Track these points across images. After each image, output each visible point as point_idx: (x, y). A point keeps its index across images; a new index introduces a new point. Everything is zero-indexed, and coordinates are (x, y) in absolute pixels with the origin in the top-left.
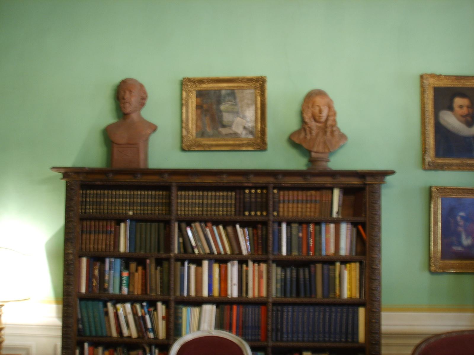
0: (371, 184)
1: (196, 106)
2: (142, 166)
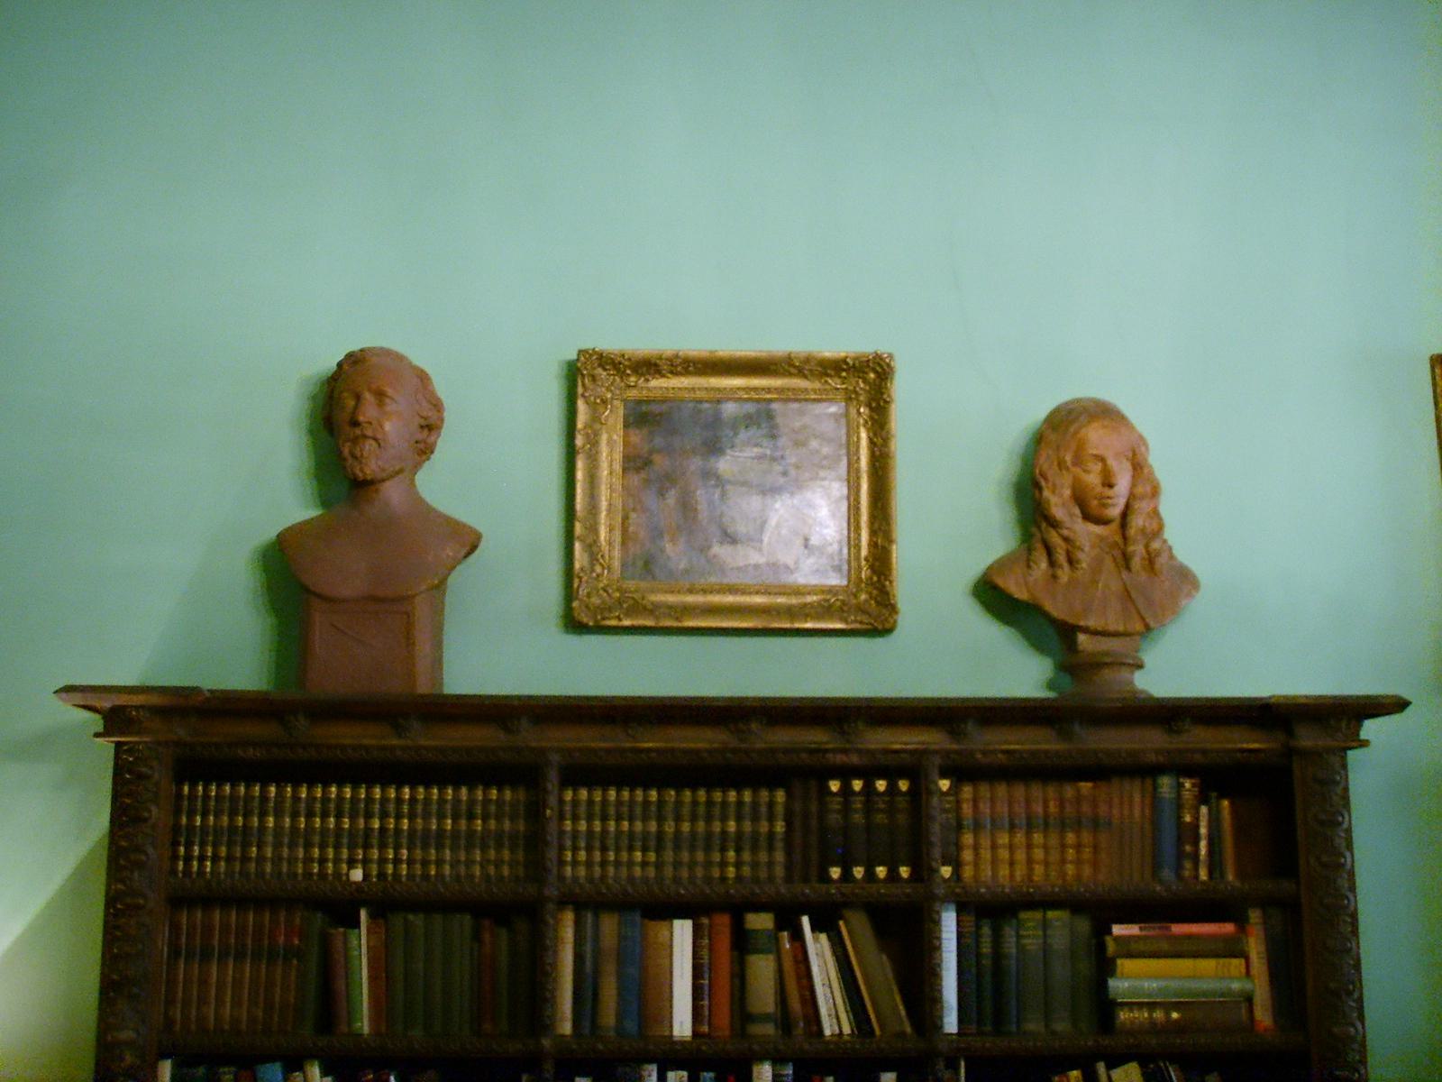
1: (624, 457)
2: (423, 688)
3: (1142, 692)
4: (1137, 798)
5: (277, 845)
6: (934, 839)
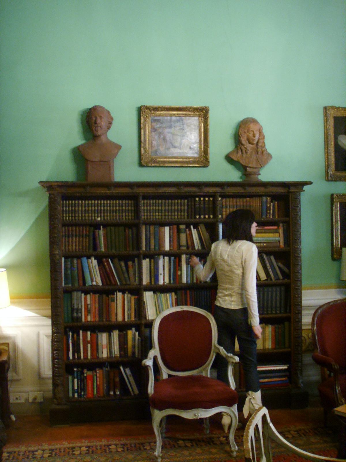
0: (294, 192)
3: (260, 180)
4: (259, 201)
5: (82, 213)
6: (218, 210)
